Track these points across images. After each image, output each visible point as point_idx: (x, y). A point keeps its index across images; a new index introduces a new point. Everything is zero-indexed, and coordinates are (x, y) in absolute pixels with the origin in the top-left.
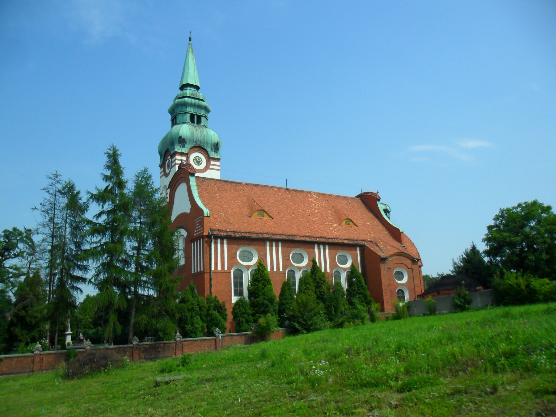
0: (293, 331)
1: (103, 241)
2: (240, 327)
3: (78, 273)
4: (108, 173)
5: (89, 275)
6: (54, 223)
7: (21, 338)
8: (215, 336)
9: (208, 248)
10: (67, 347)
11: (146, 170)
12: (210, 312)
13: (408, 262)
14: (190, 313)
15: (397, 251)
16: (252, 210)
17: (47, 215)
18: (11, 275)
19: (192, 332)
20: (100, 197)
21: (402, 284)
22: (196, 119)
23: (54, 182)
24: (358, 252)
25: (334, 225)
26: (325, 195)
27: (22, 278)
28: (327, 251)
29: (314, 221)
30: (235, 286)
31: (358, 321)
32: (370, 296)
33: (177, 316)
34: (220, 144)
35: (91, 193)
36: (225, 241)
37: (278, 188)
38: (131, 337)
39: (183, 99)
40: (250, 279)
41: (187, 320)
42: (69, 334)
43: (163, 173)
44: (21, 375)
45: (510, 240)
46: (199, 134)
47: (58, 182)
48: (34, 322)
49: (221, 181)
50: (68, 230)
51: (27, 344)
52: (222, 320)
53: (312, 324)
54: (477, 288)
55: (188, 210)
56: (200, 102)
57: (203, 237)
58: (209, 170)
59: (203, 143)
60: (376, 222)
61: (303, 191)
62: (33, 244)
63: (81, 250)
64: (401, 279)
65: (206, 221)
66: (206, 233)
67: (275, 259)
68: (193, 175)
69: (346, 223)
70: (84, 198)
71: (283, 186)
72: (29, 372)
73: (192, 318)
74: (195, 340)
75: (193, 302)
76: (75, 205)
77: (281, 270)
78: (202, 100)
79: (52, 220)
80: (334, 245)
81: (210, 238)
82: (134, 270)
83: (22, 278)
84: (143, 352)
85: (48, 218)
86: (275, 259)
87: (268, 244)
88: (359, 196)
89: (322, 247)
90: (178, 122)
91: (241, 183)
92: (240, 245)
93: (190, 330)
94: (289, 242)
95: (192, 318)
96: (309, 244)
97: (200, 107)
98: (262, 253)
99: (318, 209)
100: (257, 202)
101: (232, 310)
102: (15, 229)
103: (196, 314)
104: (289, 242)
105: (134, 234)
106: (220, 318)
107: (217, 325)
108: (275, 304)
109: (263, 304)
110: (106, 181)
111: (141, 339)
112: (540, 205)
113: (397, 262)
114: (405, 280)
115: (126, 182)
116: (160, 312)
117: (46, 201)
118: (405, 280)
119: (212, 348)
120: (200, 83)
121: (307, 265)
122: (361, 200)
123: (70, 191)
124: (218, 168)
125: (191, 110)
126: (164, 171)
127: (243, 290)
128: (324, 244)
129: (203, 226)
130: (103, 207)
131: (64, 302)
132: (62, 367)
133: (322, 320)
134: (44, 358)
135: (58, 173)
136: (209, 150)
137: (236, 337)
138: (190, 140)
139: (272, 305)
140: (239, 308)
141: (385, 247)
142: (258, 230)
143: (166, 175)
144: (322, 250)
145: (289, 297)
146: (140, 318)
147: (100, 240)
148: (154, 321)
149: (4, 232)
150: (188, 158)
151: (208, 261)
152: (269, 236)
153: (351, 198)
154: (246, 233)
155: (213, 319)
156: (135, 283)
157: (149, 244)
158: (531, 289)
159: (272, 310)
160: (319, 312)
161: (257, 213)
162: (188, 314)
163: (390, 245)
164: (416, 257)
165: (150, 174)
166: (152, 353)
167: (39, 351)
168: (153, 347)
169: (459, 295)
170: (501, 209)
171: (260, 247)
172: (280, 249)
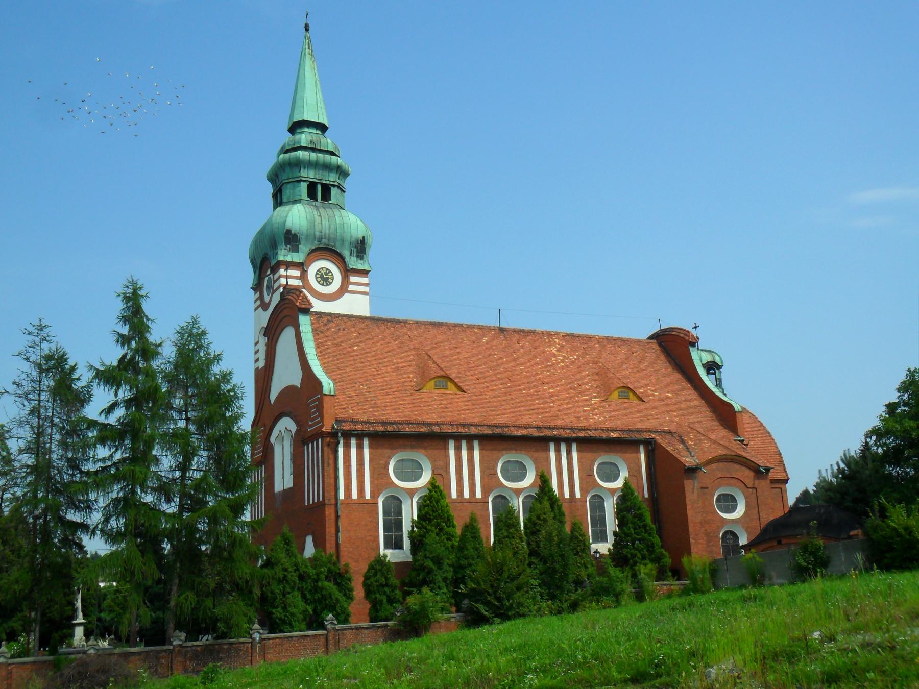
0: (475, 620)
1: (118, 456)
3: (73, 516)
4: (125, 330)
5: (96, 517)
9: (332, 456)
12: (320, 584)
13: (747, 474)
14: (281, 587)
15: (721, 451)
16: (424, 377)
17: (26, 403)
19: (284, 621)
20: (108, 377)
22: (320, 193)
23: (37, 340)
24: (642, 456)
25: (595, 401)
26: (581, 337)
28: (575, 455)
29: (552, 395)
31: (607, 600)
32: (662, 547)
34: (368, 241)
35: (95, 369)
36: (366, 442)
37: (481, 328)
38: (170, 631)
39: (293, 154)
40: (415, 518)
43: (258, 302)
46: (326, 222)
47: (45, 339)
52: (342, 599)
54: (852, 533)
55: (297, 383)
56: (328, 158)
58: (346, 295)
59: (335, 240)
61: (533, 332)
64: (733, 509)
65: (327, 403)
66: (327, 428)
67: (466, 476)
68: (306, 311)
69: (620, 397)
70: (83, 377)
71: (493, 323)
73: (284, 595)
74: (288, 638)
75: (287, 565)
76: (68, 394)
77: (479, 495)
78: (332, 153)
80: (590, 443)
84: (191, 660)
87: (452, 444)
88: (651, 338)
90: (285, 200)
91: (405, 322)
92: (395, 448)
93: (280, 619)
94: (495, 440)
95: (284, 595)
97: (327, 167)
100: (436, 359)
101: (362, 579)
104: (495, 440)
107: (332, 608)
110: (123, 345)
111: (193, 634)
113: (720, 475)
115: (160, 345)
117: (24, 376)
119: (320, 651)
120: (328, 117)
121: (532, 486)
122: (660, 344)
123: (56, 367)
124: (366, 289)
125: (310, 174)
126: (261, 298)
128: (568, 441)
129: (321, 415)
130: (116, 395)
133: (534, 598)
134: (14, 670)
135: (44, 323)
136: (346, 253)
137: (366, 631)
138: (307, 236)
140: (375, 574)
141: (699, 443)
142: (434, 417)
144: (564, 454)
147: (111, 456)
148: (209, 602)
151: (333, 481)
153: (639, 341)
155: (324, 598)
157: (202, 459)
161: (433, 382)
162: (277, 589)
163: (709, 439)
164: (762, 462)
167: (5, 657)
169: (805, 549)
170: (909, 370)
171: (436, 452)
172: (476, 453)
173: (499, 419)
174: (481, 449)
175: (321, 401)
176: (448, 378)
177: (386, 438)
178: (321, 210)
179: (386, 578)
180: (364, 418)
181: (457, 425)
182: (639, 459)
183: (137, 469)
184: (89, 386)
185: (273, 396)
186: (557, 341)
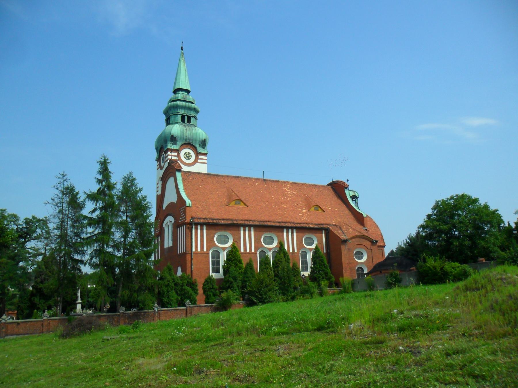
0: (250, 303)
2: (208, 299)
3: (77, 257)
4: (100, 177)
5: (87, 258)
7: (40, 306)
8: (185, 306)
9: (190, 233)
11: (131, 174)
12: (184, 287)
13: (368, 244)
15: (357, 234)
17: (57, 208)
19: (168, 303)
20: (93, 197)
21: (362, 263)
22: (186, 120)
23: (62, 181)
24: (324, 235)
25: (304, 211)
26: (299, 184)
27: (40, 258)
29: (285, 208)
31: (307, 295)
32: (331, 273)
33: (156, 290)
34: (207, 141)
36: (205, 227)
37: (255, 179)
39: (175, 102)
40: (225, 260)
41: (164, 294)
44: (33, 335)
45: (440, 228)
46: (189, 132)
47: (65, 180)
49: (207, 174)
52: (193, 294)
53: (266, 297)
54: (411, 269)
56: (190, 104)
57: (185, 224)
58: (197, 164)
60: (344, 207)
61: (278, 181)
62: (49, 229)
63: (81, 238)
64: (361, 258)
65: (188, 210)
67: (248, 242)
68: (179, 170)
70: (82, 197)
71: (261, 177)
72: (40, 333)
77: (253, 251)
78: (192, 103)
79: (61, 212)
80: (301, 229)
81: (190, 225)
83: (40, 258)
88: (328, 185)
89: (290, 231)
90: (171, 122)
91: (222, 176)
94: (261, 227)
95: (168, 292)
96: (279, 228)
97: (190, 109)
98: (237, 237)
99: (290, 197)
101: (202, 286)
102: (34, 217)
103: (172, 289)
104: (261, 227)
107: (189, 298)
108: (238, 281)
109: (228, 281)
110: (99, 184)
112: (469, 197)
114: (365, 259)
115: (115, 184)
116: (140, 288)
118: (365, 259)
121: (276, 247)
122: (332, 188)
123: (70, 193)
124: (206, 161)
125: (182, 112)
126: (160, 164)
127: (219, 268)
128: (292, 228)
129: (185, 215)
130: (96, 205)
132: (61, 329)
133: (276, 295)
134: (51, 322)
136: (197, 146)
137: (203, 308)
138: (180, 139)
139: (236, 281)
140: (208, 284)
141: (348, 229)
142: (234, 217)
143: (161, 168)
144: (290, 234)
145: (251, 275)
147: (94, 231)
148: (135, 295)
149: (25, 220)
151: (190, 244)
152: (243, 222)
153: (323, 186)
154: (223, 219)
155: (185, 293)
156: (111, 269)
157: (133, 233)
158: (444, 271)
160: (274, 288)
161: (234, 202)
162: (165, 289)
164: (374, 238)
165: (134, 177)
168: (135, 314)
169: (391, 275)
172: (252, 233)
173: (263, 218)
174: (254, 231)
175: (185, 209)
177: (213, 226)
178: (187, 127)
179: (213, 286)
182: (322, 236)
183: (105, 237)
184: (84, 201)
185: (164, 207)
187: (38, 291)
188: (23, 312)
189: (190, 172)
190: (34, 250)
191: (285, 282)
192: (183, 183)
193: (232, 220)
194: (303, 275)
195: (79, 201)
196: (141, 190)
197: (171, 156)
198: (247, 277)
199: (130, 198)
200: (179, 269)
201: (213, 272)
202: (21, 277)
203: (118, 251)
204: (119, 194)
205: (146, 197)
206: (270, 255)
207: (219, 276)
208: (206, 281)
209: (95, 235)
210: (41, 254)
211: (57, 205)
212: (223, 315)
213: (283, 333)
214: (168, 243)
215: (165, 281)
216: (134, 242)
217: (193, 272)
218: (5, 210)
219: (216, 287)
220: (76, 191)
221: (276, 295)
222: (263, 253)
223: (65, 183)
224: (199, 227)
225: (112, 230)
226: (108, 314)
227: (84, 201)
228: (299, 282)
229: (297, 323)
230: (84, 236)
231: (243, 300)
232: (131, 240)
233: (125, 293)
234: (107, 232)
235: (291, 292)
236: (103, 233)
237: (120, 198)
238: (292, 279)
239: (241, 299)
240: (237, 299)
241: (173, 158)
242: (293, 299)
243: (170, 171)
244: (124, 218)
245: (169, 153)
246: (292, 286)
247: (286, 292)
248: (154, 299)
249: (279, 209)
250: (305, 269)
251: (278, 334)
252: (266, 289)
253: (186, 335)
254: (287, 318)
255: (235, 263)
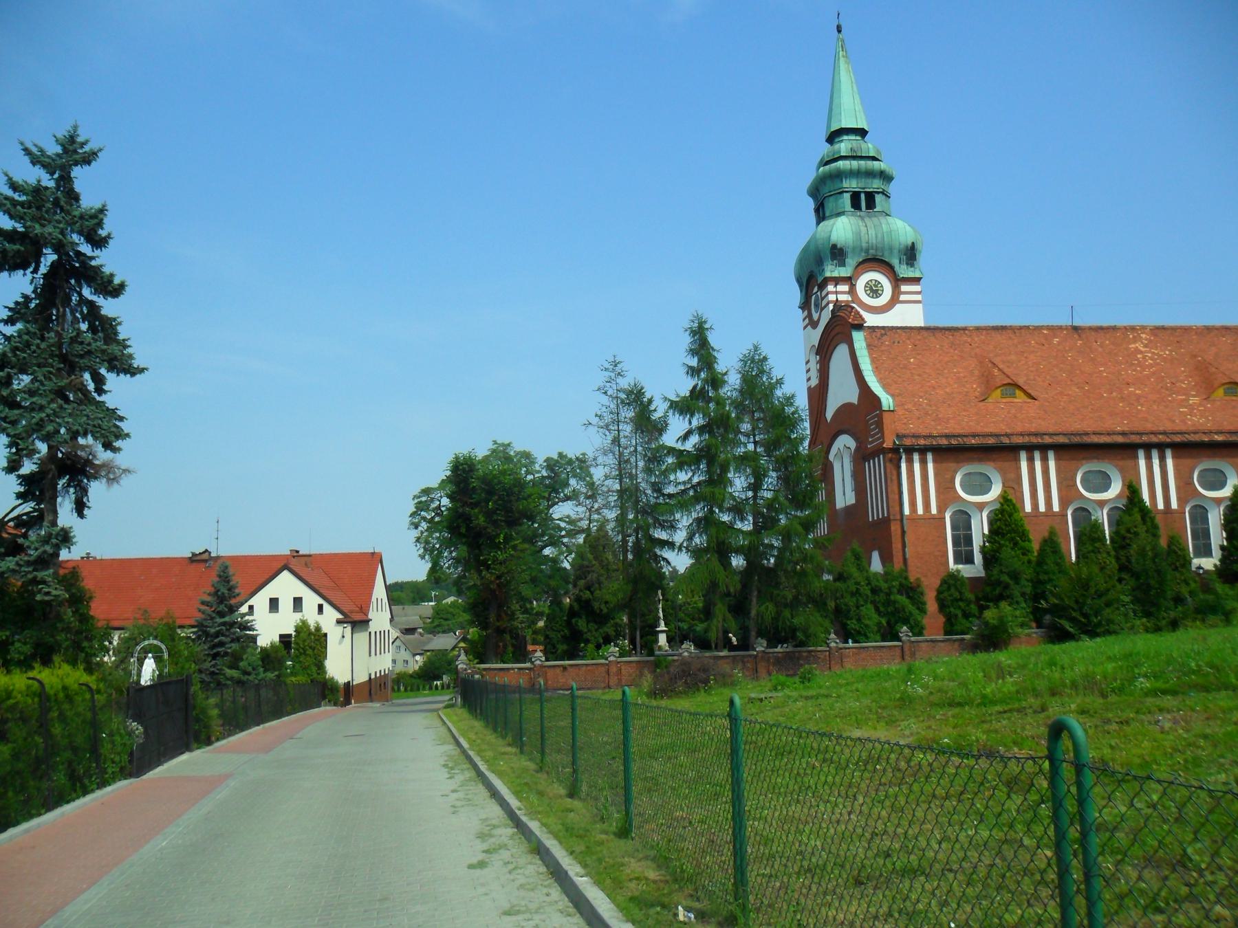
0: (1059, 636)
1: (696, 480)
2: (952, 625)
3: (661, 535)
4: (694, 362)
5: (680, 537)
6: (619, 446)
7: (588, 636)
8: (899, 639)
9: (895, 472)
10: (657, 653)
11: (756, 348)
12: (892, 597)
16: (988, 386)
18: (563, 533)
19: (859, 633)
20: (683, 407)
22: (864, 202)
23: (613, 375)
25: (1193, 400)
26: (1174, 329)
27: (581, 539)
29: (1138, 398)
30: (955, 544)
31: (1212, 619)
33: (831, 604)
34: (919, 246)
36: (930, 457)
37: (1049, 328)
40: (986, 532)
41: (849, 611)
42: (662, 632)
46: (872, 232)
48: (605, 610)
50: (641, 464)
51: (598, 647)
52: (915, 612)
53: (1100, 622)
56: (870, 163)
57: (883, 451)
58: (898, 306)
59: (883, 249)
61: (1114, 328)
63: (664, 495)
65: (887, 419)
66: (888, 444)
67: (1040, 488)
68: (859, 327)
70: (659, 409)
71: (1064, 321)
73: (858, 607)
75: (859, 579)
76: (648, 425)
77: (1056, 508)
78: (874, 159)
79: (616, 441)
80: (1186, 448)
81: (895, 454)
82: (750, 528)
85: (610, 438)
86: (1040, 488)
87: (1023, 456)
90: (827, 214)
91: (965, 329)
94: (1073, 450)
95: (858, 607)
97: (870, 174)
98: (1012, 476)
99: (1151, 366)
100: (1001, 366)
102: (560, 454)
103: (866, 602)
104: (1073, 450)
105: (745, 459)
106: (911, 608)
107: (906, 621)
108: (1023, 582)
109: (999, 583)
115: (726, 374)
116: (796, 598)
120: (868, 124)
121: (1119, 497)
123: (636, 398)
124: (918, 297)
125: (852, 184)
126: (810, 316)
127: (972, 551)
129: (882, 431)
130: (690, 423)
131: (645, 578)
133: (1126, 615)
136: (895, 262)
137: (942, 644)
138: (854, 249)
139: (1017, 583)
140: (949, 588)
142: (1003, 428)
143: (814, 324)
144: (917, 466)
145: (1056, 569)
146: (763, 608)
150: (852, 291)
152: (1026, 439)
154: (974, 436)
155: (897, 611)
159: (1017, 593)
160: (1118, 600)
162: (851, 601)
166: (789, 665)
168: (788, 655)
173: (1077, 426)
174: (934, 461)
175: (880, 417)
176: (1016, 386)
177: (951, 452)
178: (867, 220)
179: (961, 593)
180: (925, 432)
181: (1029, 435)
184: (665, 416)
185: (829, 415)
186: (1143, 336)
187: (585, 607)
188: (554, 647)
189: (883, 328)
190: (568, 523)
191: (1149, 586)
192: (870, 355)
193: (997, 436)
194: (1199, 568)
195: (656, 416)
196: (780, 382)
197: (836, 293)
198: (1046, 573)
199: (759, 401)
200: (876, 556)
201: (956, 561)
202: (550, 577)
203: (742, 519)
204: (735, 394)
205: (793, 396)
206: (1103, 516)
207: (975, 569)
208: (944, 582)
209: (693, 487)
210: (582, 531)
211: (607, 426)
212: (1002, 657)
213: (1165, 692)
214: (845, 497)
215: (851, 583)
216: (775, 499)
217: (910, 562)
218: (509, 445)
219: (970, 596)
220: (648, 395)
221: (1126, 615)
222: (1082, 514)
223: (620, 380)
224: (916, 457)
225: (729, 475)
226: (732, 653)
227: (665, 416)
228: (1188, 584)
229: (1198, 672)
230: (670, 490)
231: (1038, 627)
232: (769, 495)
233: (767, 608)
234: (717, 480)
235: (1167, 609)
236: (710, 482)
237: (738, 405)
238: (1169, 577)
239: (1034, 625)
240: (1022, 625)
241: (842, 298)
242: (1174, 625)
243: (839, 329)
244: (751, 447)
245: (830, 288)
246: (1169, 594)
247: (1153, 609)
248: (827, 623)
249: (1122, 399)
250: (1206, 551)
251: (1154, 693)
252: (1100, 602)
253: (931, 693)
254: (1170, 660)
255: (1012, 539)
